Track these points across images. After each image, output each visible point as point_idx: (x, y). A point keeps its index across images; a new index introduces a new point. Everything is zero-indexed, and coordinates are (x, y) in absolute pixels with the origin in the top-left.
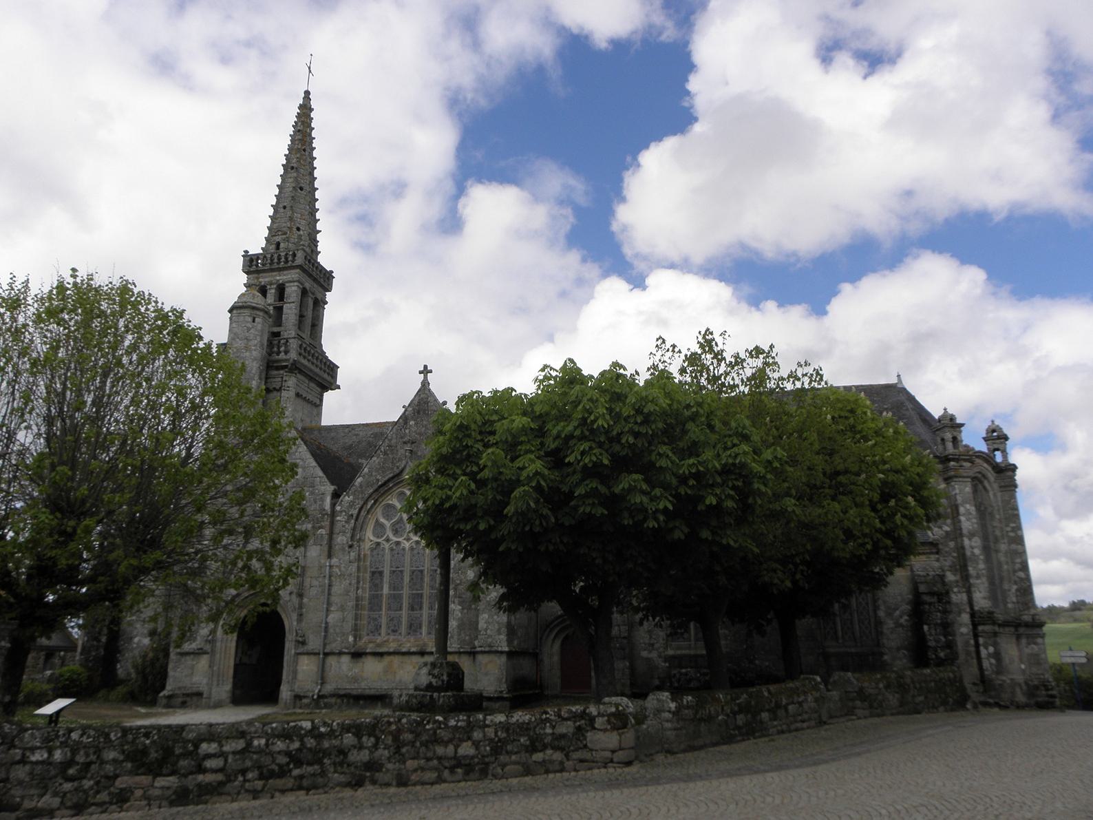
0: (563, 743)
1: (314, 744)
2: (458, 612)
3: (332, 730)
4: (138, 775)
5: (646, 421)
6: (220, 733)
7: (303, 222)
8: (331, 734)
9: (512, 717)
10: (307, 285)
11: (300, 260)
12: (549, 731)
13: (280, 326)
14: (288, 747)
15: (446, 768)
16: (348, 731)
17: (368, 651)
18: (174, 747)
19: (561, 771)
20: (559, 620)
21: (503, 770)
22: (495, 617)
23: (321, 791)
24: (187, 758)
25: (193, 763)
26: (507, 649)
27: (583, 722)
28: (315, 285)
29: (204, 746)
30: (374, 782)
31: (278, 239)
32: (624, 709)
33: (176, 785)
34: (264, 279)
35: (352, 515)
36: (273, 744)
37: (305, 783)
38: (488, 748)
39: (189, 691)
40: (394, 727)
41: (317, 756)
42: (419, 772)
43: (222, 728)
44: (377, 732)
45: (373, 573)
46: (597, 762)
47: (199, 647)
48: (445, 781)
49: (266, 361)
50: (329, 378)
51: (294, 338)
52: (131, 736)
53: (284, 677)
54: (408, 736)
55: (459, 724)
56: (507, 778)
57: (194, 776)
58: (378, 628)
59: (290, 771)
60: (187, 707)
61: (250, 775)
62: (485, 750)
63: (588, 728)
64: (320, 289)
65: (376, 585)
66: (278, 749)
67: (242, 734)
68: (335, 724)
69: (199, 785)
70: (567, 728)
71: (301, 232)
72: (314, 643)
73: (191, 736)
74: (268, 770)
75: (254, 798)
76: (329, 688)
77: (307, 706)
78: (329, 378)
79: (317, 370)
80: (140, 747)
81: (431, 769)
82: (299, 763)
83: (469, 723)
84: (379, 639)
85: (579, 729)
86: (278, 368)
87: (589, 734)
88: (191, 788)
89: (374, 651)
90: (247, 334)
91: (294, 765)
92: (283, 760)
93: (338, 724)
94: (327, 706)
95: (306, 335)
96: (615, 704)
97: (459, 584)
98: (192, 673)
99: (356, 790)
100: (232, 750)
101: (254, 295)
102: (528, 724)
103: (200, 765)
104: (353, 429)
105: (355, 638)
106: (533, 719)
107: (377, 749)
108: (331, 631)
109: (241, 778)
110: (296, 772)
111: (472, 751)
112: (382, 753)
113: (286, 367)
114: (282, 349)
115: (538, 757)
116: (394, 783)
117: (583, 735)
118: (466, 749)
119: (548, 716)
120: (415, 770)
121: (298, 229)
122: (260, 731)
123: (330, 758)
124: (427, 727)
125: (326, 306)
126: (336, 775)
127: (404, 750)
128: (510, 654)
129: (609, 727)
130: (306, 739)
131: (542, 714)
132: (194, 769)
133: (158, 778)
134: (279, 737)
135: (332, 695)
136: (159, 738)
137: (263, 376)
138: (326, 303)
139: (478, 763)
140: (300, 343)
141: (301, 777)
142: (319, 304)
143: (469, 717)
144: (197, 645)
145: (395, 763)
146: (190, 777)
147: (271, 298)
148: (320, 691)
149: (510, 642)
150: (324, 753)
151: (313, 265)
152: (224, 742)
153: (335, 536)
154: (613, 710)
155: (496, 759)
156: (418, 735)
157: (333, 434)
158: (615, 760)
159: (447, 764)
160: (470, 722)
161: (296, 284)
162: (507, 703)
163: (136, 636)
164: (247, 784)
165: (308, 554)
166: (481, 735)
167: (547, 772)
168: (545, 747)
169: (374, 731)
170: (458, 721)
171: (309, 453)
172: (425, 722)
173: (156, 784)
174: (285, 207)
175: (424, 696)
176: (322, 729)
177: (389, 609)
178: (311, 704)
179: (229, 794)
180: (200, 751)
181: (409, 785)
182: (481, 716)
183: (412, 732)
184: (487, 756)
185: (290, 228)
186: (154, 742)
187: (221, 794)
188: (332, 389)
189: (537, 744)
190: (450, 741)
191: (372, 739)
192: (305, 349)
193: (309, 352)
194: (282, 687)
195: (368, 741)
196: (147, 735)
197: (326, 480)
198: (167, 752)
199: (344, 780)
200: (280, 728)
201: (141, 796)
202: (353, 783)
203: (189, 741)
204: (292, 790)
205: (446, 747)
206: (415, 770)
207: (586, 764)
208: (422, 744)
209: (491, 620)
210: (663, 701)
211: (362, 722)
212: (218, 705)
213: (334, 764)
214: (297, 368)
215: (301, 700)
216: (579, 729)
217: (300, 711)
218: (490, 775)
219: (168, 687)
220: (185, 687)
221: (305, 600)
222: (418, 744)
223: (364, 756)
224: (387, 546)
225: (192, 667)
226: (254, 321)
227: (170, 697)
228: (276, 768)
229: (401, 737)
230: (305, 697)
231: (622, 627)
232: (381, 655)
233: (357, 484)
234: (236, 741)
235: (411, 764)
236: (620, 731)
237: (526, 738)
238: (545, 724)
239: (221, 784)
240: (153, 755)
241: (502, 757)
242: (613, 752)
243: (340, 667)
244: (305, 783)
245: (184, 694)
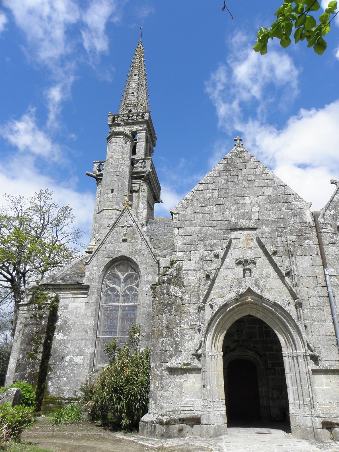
13: (135, 155)
20: (305, 358)
47: (185, 362)
98: (181, 392)
113: (143, 177)
163: (68, 354)
174: (133, 93)
226: (126, 143)
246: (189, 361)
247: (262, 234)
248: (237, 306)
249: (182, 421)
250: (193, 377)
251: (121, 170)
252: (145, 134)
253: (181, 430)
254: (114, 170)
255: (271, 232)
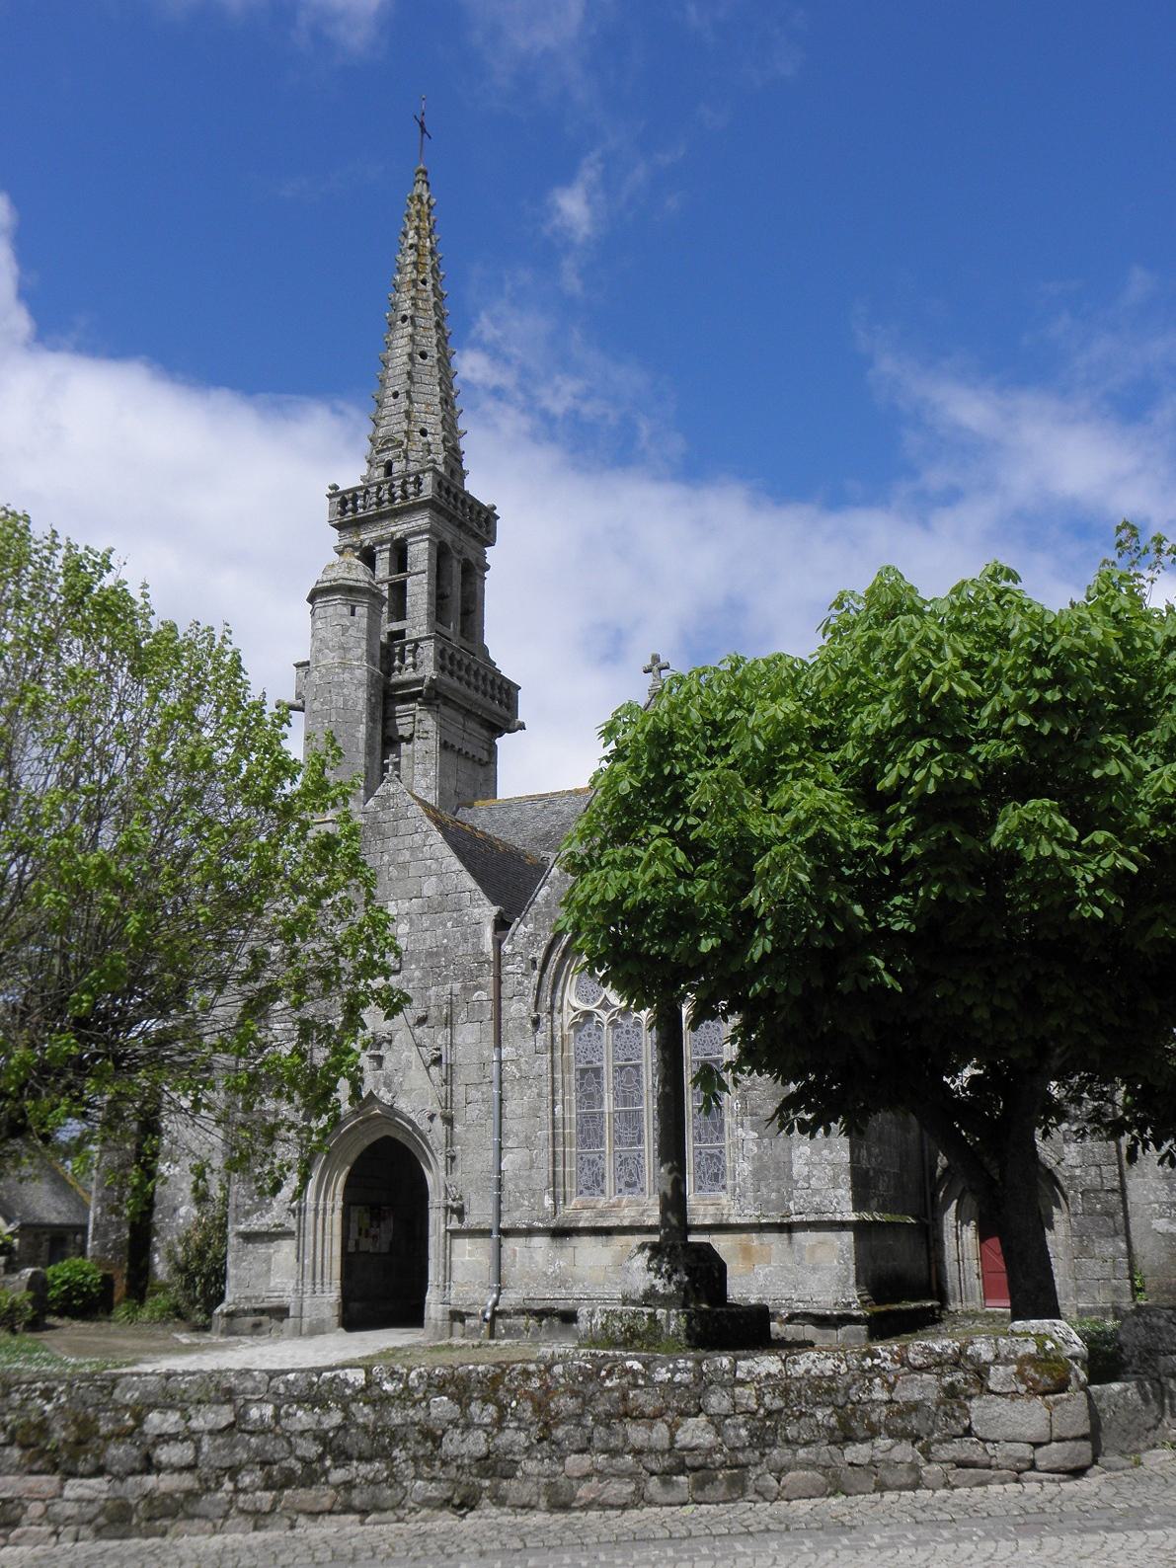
0: (914, 1422)
1: (372, 1417)
2: (751, 1145)
3: (407, 1388)
4: (31, 1473)
5: (1061, 679)
6: (185, 1391)
7: (432, 419)
8: (406, 1396)
9: (795, 1362)
10: (448, 538)
11: (428, 491)
12: (880, 1394)
14: (319, 1422)
15: (653, 1473)
16: (441, 1390)
17: (581, 1225)
18: (97, 1419)
19: (915, 1486)
21: (779, 1481)
22: (825, 1152)
23: (390, 1515)
24: (123, 1443)
25: (135, 1452)
26: (853, 1217)
27: (960, 1375)
28: (463, 536)
29: (154, 1417)
30: (499, 1501)
31: (387, 456)
32: (1059, 1348)
33: (104, 1496)
34: (368, 536)
35: (534, 961)
36: (288, 1415)
37: (357, 1498)
38: (743, 1432)
39: (264, 1305)
40: (536, 1383)
41: (381, 1444)
42: (595, 1479)
43: (190, 1382)
44: (501, 1393)
45: (583, 1072)
46: (998, 1468)
47: (277, 1221)
48: (651, 1503)
49: (380, 686)
50: (503, 711)
51: (429, 638)
52: (17, 1396)
53: (431, 1277)
54: (566, 1404)
55: (678, 1378)
56: (788, 1500)
57: (139, 1478)
58: (598, 1181)
59: (326, 1472)
60: (263, 1333)
61: (246, 1480)
62: (738, 1436)
63: (973, 1391)
64: (473, 542)
65: (590, 1096)
66: (300, 1427)
67: (229, 1396)
68: (413, 1375)
69: (148, 1496)
70: (923, 1389)
71: (429, 438)
72: (480, 1214)
73: (130, 1397)
74: (281, 1469)
75: (256, 1528)
76: (511, 1298)
77: (475, 1331)
78: (503, 711)
79: (478, 696)
80: (34, 1418)
81: (619, 1475)
82: (343, 1457)
83: (700, 1375)
84: (602, 1202)
85: (951, 1392)
86: (405, 699)
87: (974, 1403)
88: (133, 1502)
89: (593, 1224)
90: (343, 639)
91: (334, 1460)
92: (311, 1449)
93: (420, 1376)
94: (510, 1332)
95: (452, 629)
96: (1038, 1335)
97: (749, 1089)
98: (269, 1270)
99: (463, 1516)
100: (208, 1427)
101: (349, 566)
102: (832, 1379)
103: (148, 1458)
104: (551, 802)
105: (555, 1199)
106: (843, 1368)
107: (501, 1429)
108: (509, 1186)
109: (228, 1485)
110: (338, 1475)
111: (707, 1438)
112: (514, 1437)
114: (409, 660)
115: (858, 1452)
116: (543, 1503)
117: (962, 1407)
118: (695, 1433)
119: (876, 1361)
120: (587, 1477)
121: (424, 433)
122: (264, 1388)
123: (405, 1448)
124: (608, 1384)
125: (486, 574)
126: (419, 1483)
127: (559, 1433)
128: (859, 1228)
129: (1022, 1388)
130: (353, 1407)
131: (864, 1356)
132: (137, 1465)
133: (71, 1482)
134: (300, 1401)
135: (522, 1312)
136: (69, 1400)
137: (379, 714)
138: (487, 568)
139: (723, 1466)
140: (440, 646)
141: (349, 1485)
142: (474, 571)
143: (699, 1362)
144: (273, 1218)
145: (542, 1460)
146: (131, 1480)
147: (383, 568)
148: (496, 1304)
149: (859, 1203)
150: (393, 1437)
151: (456, 497)
152: (191, 1411)
153: (504, 1003)
154: (1032, 1348)
155: (763, 1455)
156: (587, 1401)
157: (515, 815)
158: (1041, 1464)
159: (654, 1466)
160: (703, 1373)
161: (426, 536)
162: (862, 1329)
164: (242, 1497)
165: (458, 1040)
166: (726, 1403)
167: (881, 1487)
168: (873, 1432)
169: (496, 1391)
170: (674, 1371)
171: (446, 845)
172: (603, 1373)
173: (68, 1493)
175: (635, 1315)
176: (388, 1387)
177: (618, 1141)
178: (481, 1328)
179: (206, 1517)
180: (145, 1427)
181: (575, 1509)
182: (725, 1361)
183: (575, 1394)
184: (743, 1449)
185: (407, 433)
186: (59, 1408)
187: (191, 1517)
188: (510, 731)
189: (854, 1424)
190: (659, 1414)
191: (492, 1408)
192: (452, 658)
193: (460, 663)
194: (428, 1297)
195: (485, 1414)
196: (47, 1394)
197: (482, 896)
198: (85, 1435)
199: (435, 1494)
200: (302, 1383)
201: (41, 1517)
202: (457, 1501)
203: (126, 1407)
204: (331, 1512)
205: (651, 1428)
206: (587, 1477)
207: (972, 1470)
208: (597, 1420)
209: (816, 1159)
210: (1159, 1328)
211: (470, 1371)
212: (317, 1330)
213: (415, 1459)
214: (438, 695)
215: (462, 1321)
216: (951, 1392)
217: (463, 1342)
218: (751, 1490)
219: (229, 1298)
220: (256, 1298)
221: (458, 1128)
222: (589, 1420)
223: (476, 1443)
224: (605, 1016)
225: (268, 1260)
226: (353, 614)
227: (230, 1315)
228: (298, 1466)
229: (552, 1405)
230: (469, 1315)
231: (1104, 1168)
232: (607, 1232)
233: (539, 899)
234: (215, 1407)
235: (576, 1463)
236: (1050, 1398)
237: (828, 1411)
238: (871, 1380)
239: (191, 1494)
240: (60, 1434)
241: (775, 1452)
242: (1036, 1445)
243: (531, 1257)
244: (357, 1498)
245: (255, 1310)
246: (281, 1221)
247: (409, 981)
248: (361, 1122)
249: (262, 1312)
250: (287, 1247)
251: (340, 704)
252: (426, 544)
253: (257, 1326)
254: (322, 704)
255: (423, 978)
